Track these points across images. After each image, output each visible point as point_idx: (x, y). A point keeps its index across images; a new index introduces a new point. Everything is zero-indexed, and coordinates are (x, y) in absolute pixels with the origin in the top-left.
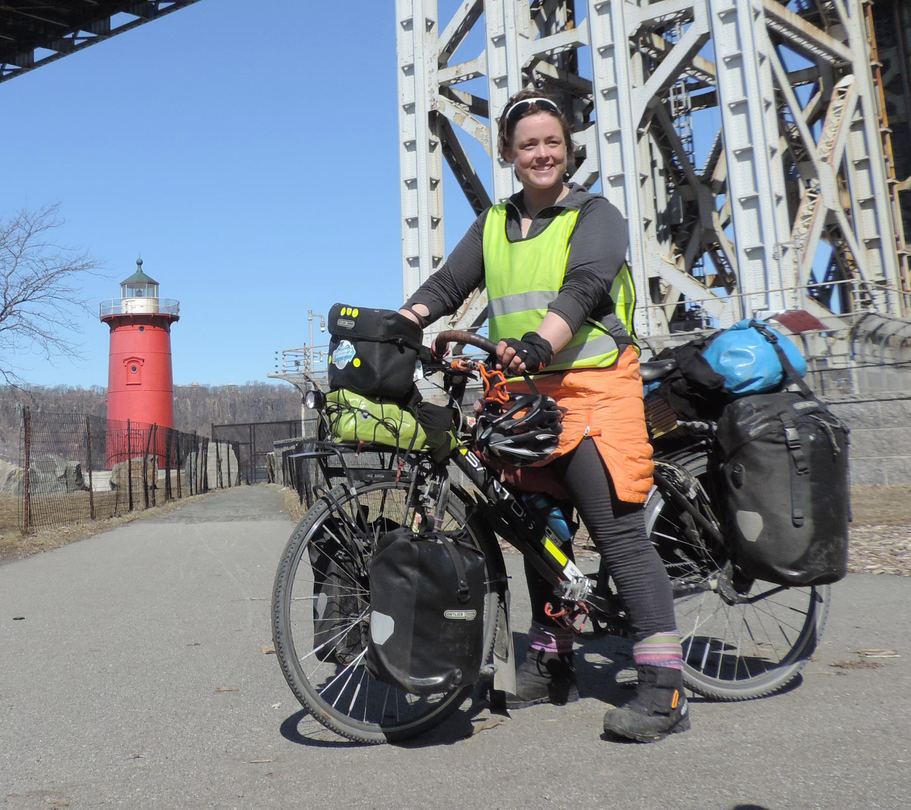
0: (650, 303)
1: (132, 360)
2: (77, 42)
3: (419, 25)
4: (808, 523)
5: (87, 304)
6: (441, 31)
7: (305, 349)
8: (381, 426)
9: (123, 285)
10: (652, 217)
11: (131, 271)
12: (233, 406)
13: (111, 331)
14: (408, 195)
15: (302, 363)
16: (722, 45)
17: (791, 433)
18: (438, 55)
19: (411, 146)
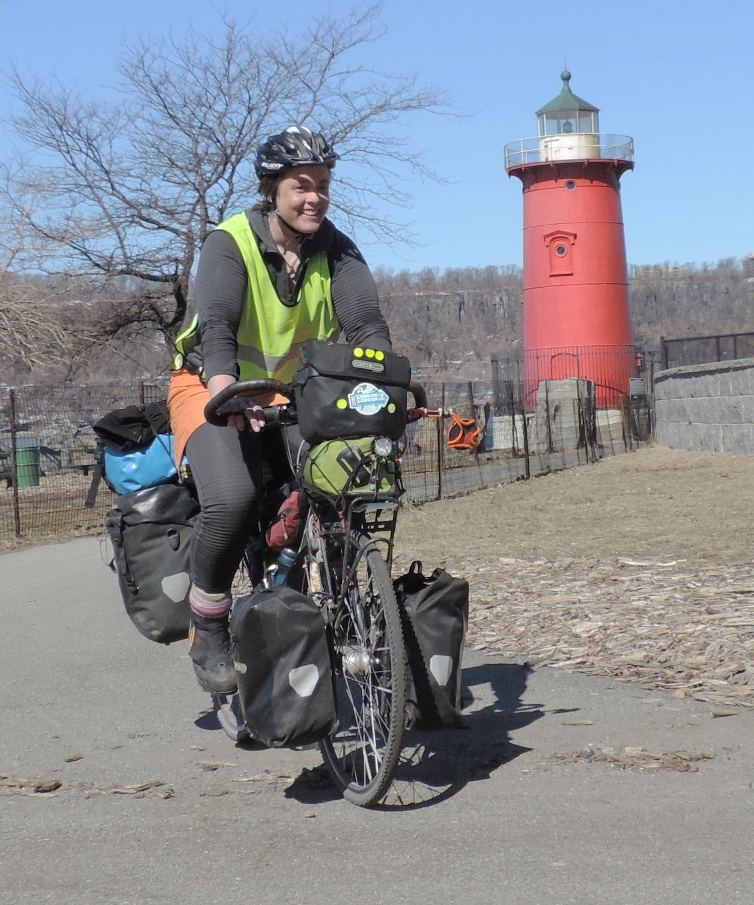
1: (556, 236)
5: (418, 160)
9: (539, 114)
11: (553, 90)
13: (524, 190)
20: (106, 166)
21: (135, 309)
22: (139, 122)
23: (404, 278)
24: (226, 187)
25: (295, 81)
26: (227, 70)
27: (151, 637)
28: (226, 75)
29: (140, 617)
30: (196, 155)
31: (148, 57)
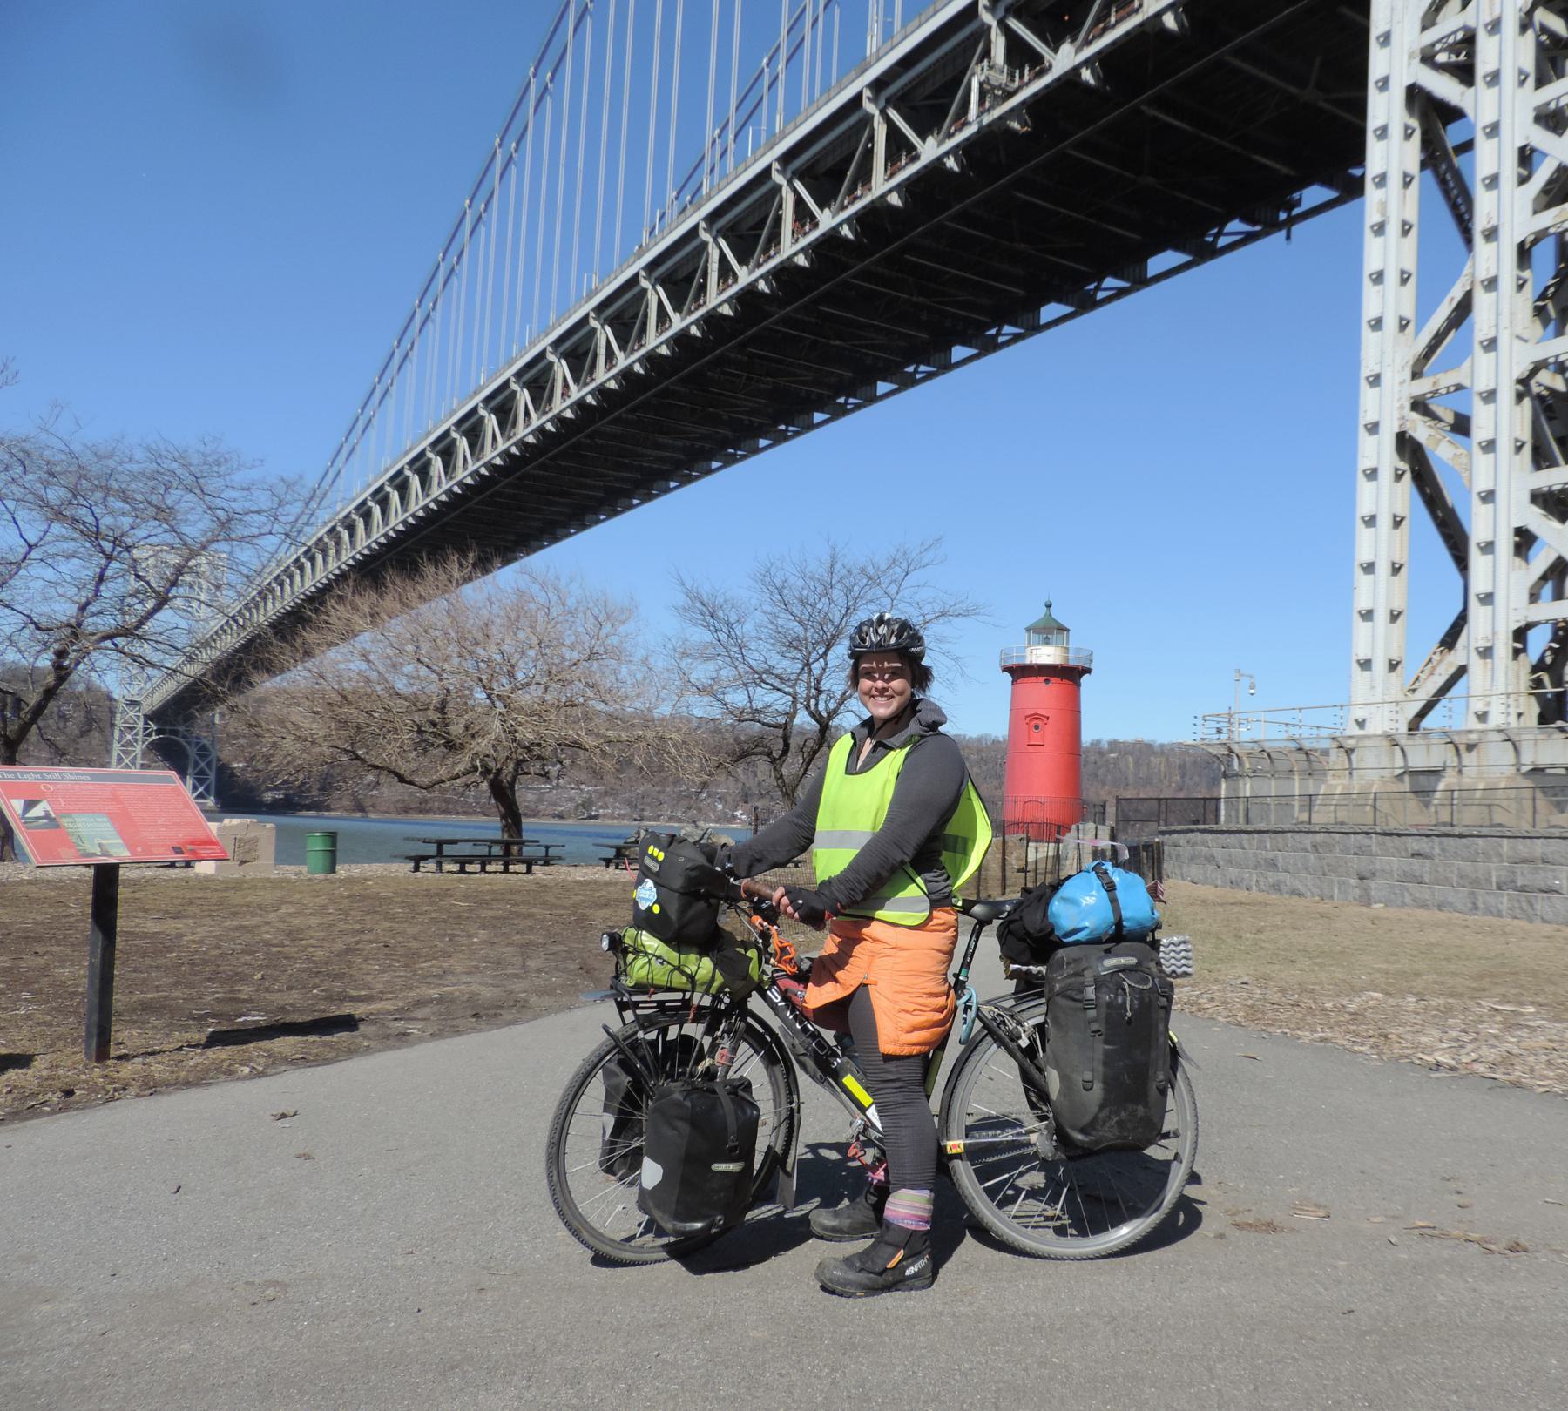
1: (1035, 717)
2: (1001, 339)
3: (1390, 324)
4: (1098, 1088)
7: (1230, 715)
8: (676, 972)
9: (1028, 630)
11: (1039, 614)
12: (1182, 767)
14: (1364, 534)
15: (1225, 730)
17: (1090, 992)
18: (1411, 363)
19: (1372, 474)
31: (773, 571)
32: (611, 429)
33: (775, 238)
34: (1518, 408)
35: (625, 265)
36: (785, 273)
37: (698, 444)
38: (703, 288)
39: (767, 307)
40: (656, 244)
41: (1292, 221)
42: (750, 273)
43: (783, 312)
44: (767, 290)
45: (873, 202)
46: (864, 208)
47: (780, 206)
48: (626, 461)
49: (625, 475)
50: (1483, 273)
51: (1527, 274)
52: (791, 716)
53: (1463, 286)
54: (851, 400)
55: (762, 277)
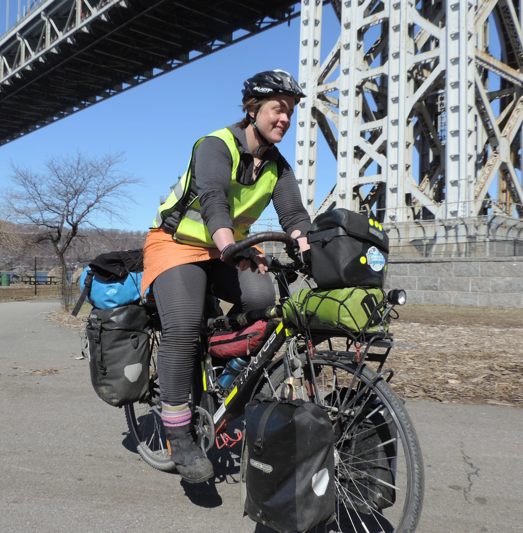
0: (405, 205)
3: (310, 62)
6: (321, 65)
10: (474, 153)
16: (450, 76)
18: (318, 78)
20: (39, 193)
21: (45, 236)
22: (50, 181)
23: (131, 233)
24: (75, 201)
25: (98, 173)
26: (78, 167)
27: (111, 404)
28: (77, 169)
29: (104, 389)
30: (67, 191)
31: (54, 161)
32: (8, 102)
33: (73, 20)
34: (357, 98)
35: (10, 30)
36: (78, 35)
37: (47, 109)
38: (44, 41)
39: (72, 50)
40: (23, 21)
41: (290, 17)
42: (64, 35)
43: (79, 52)
44: (71, 43)
45: (114, 5)
46: (110, 7)
47: (75, 6)
48: (16, 116)
49: (16, 122)
50: (344, 43)
51: (361, 43)
52: (62, 223)
53: (337, 47)
54: (112, 91)
55: (69, 36)
